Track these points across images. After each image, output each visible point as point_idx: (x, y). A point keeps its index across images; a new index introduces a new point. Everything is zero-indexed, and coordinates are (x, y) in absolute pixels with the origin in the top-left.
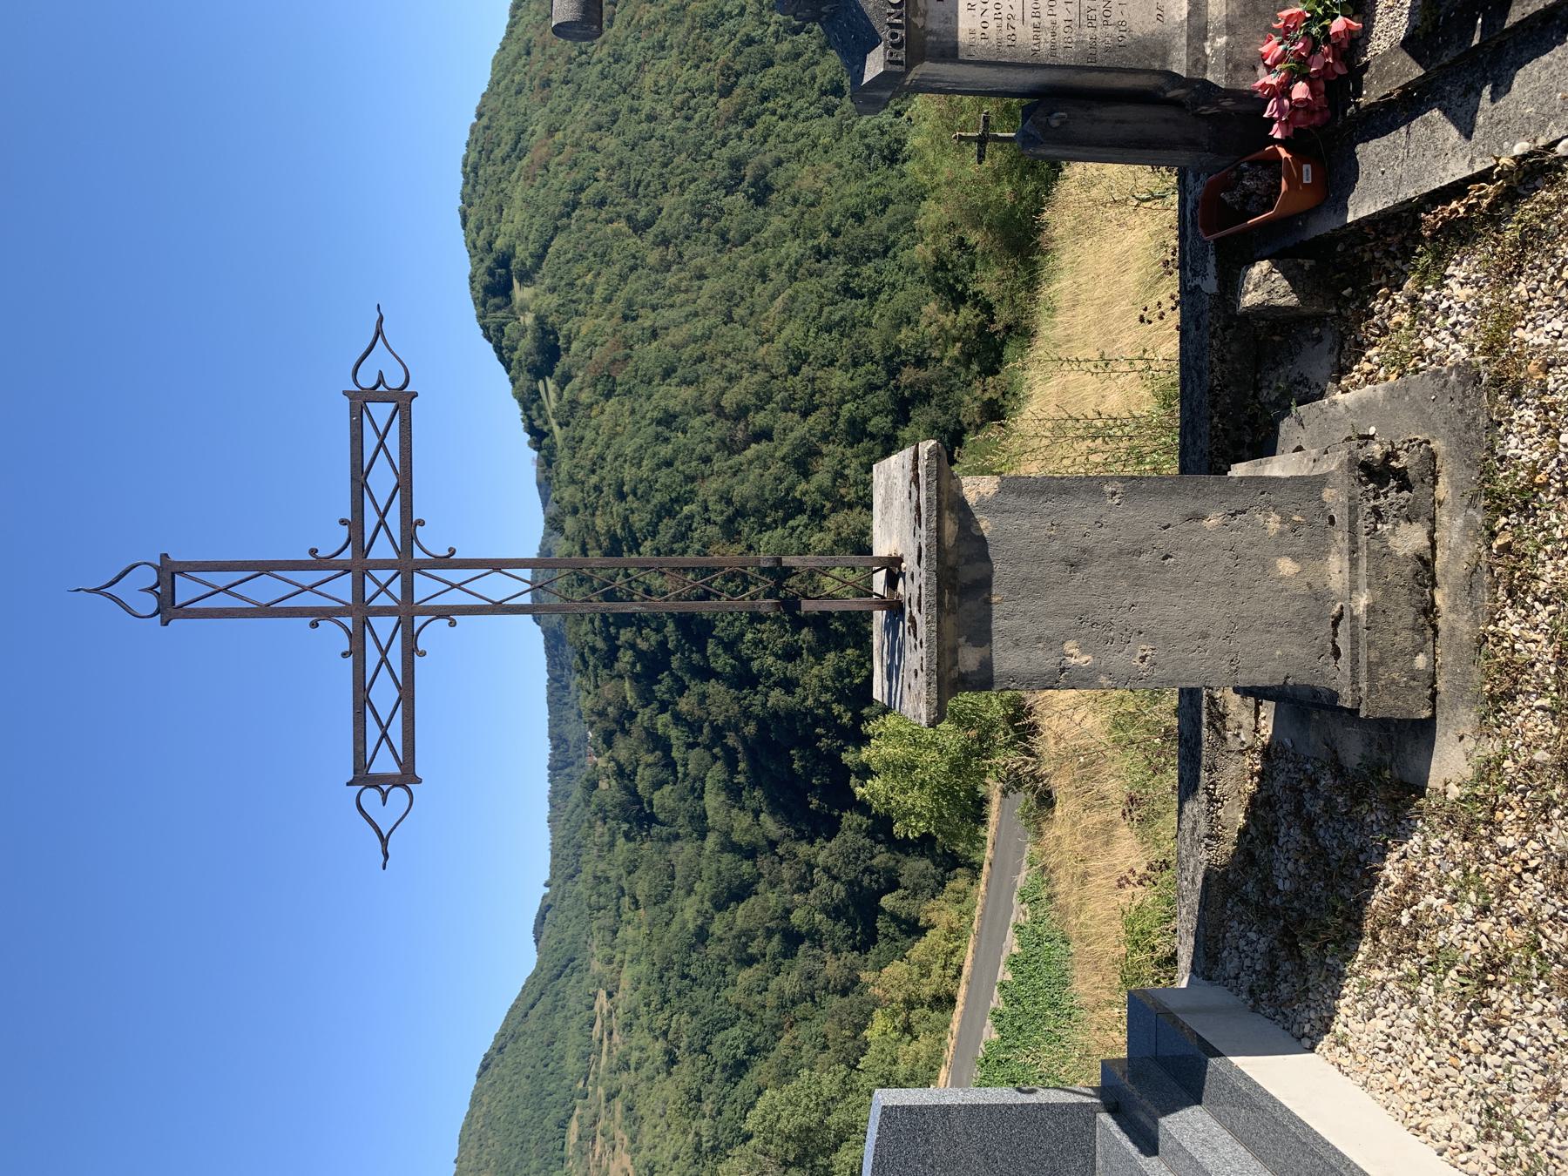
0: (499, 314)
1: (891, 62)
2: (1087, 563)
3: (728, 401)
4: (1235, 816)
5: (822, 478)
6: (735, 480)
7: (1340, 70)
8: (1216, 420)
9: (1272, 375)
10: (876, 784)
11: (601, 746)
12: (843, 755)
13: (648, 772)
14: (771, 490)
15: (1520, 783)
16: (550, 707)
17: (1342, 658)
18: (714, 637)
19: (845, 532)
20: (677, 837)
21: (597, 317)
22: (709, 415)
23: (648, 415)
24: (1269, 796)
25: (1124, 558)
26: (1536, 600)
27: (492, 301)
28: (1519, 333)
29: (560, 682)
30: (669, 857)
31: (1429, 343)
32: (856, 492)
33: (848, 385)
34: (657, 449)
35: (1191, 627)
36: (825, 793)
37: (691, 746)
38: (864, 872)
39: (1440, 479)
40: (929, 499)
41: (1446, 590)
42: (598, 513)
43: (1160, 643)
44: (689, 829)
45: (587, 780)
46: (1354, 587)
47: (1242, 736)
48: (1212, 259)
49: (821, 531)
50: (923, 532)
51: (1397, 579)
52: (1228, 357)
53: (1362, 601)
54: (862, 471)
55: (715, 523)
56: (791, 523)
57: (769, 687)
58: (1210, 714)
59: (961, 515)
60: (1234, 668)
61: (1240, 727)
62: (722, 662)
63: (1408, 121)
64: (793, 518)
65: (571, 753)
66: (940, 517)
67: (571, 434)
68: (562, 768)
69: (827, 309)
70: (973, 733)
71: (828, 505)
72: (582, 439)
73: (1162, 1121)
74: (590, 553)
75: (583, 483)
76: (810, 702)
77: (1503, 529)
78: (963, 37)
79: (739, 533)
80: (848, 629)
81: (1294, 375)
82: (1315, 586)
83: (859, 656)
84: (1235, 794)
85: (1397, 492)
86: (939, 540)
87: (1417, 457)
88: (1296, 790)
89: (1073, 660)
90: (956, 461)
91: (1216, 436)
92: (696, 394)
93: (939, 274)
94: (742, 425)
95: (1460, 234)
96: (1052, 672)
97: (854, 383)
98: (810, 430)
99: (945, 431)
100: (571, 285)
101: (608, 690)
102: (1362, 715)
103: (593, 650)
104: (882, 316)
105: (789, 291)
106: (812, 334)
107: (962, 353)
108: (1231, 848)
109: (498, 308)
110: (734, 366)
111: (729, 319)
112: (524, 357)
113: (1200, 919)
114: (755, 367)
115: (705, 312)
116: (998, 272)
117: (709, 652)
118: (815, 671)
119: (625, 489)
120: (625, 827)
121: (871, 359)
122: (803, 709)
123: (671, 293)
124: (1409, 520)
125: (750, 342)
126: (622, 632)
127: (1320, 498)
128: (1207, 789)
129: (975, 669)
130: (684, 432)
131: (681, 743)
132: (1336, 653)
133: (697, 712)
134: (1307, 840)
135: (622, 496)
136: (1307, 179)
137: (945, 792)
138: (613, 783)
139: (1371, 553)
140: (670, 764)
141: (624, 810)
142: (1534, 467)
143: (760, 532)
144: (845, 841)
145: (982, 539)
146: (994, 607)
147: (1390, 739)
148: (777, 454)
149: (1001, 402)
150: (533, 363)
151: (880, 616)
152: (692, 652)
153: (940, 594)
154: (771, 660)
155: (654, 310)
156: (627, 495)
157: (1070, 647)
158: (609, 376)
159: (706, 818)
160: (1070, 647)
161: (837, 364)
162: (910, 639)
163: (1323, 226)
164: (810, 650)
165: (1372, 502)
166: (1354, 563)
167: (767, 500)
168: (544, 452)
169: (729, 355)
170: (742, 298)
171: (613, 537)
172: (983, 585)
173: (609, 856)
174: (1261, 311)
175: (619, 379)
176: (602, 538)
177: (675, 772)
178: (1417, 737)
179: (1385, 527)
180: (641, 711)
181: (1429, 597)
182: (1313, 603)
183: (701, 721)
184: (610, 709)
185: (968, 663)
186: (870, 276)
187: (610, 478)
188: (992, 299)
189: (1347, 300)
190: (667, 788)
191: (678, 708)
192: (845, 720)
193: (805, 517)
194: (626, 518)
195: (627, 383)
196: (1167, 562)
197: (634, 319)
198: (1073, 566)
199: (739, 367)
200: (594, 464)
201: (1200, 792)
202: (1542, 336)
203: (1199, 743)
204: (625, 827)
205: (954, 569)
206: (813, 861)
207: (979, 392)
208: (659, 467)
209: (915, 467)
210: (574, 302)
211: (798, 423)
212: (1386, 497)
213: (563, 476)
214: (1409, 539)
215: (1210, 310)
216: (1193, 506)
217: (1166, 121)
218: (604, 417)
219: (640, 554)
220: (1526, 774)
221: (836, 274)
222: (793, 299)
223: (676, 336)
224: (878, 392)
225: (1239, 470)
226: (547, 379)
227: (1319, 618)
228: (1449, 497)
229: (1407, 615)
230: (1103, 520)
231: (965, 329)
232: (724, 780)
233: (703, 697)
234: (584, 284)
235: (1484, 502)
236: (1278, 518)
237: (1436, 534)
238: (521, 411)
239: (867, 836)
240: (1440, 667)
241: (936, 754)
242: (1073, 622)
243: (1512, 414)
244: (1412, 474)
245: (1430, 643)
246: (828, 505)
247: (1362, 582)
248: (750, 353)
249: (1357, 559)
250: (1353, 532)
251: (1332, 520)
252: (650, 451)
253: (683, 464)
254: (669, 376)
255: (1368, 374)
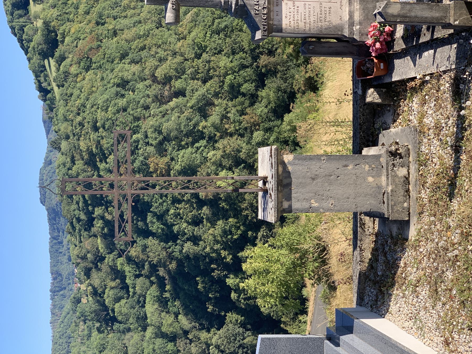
0: (21, 20)
1: (263, 35)
2: (317, 178)
3: (159, 73)
4: (368, 255)
5: (214, 118)
6: (164, 120)
7: (389, 39)
8: (361, 133)
9: (378, 120)
10: (250, 282)
11: (83, 277)
12: (227, 280)
13: (111, 292)
14: (185, 125)
16: (51, 255)
18: (151, 212)
19: (228, 150)
20: (129, 330)
21: (81, 23)
22: (148, 81)
23: (112, 81)
27: (17, 12)
29: (57, 240)
30: (124, 342)
32: (235, 127)
33: (229, 65)
34: (117, 101)
35: (345, 196)
36: (217, 302)
37: (137, 276)
38: (239, 348)
40: (275, 162)
42: (81, 139)
43: (336, 200)
44: (136, 325)
45: (74, 298)
46: (388, 185)
48: (360, 84)
49: (214, 150)
50: (273, 170)
51: (399, 183)
52: (365, 114)
53: (390, 188)
54: (238, 114)
55: (152, 145)
56: (197, 145)
57: (184, 241)
58: (360, 223)
62: (156, 227)
63: (404, 57)
64: (197, 141)
65: (63, 282)
66: (278, 166)
67: (65, 91)
68: (58, 291)
69: (217, 21)
70: (298, 255)
71: (218, 134)
72: (71, 95)
73: (342, 337)
74: (76, 162)
75: (72, 121)
76: (208, 249)
78: (284, 26)
79: (166, 151)
80: (230, 206)
81: (383, 121)
83: (236, 223)
86: (278, 172)
87: (404, 150)
88: (383, 245)
89: (313, 205)
90: (291, 111)
92: (140, 69)
94: (167, 87)
95: (415, 90)
96: (308, 208)
99: (285, 92)
101: (88, 244)
103: (79, 220)
107: (294, 51)
108: (367, 265)
109: (21, 16)
111: (159, 25)
112: (36, 46)
113: (358, 288)
114: (175, 54)
117: (148, 221)
118: (211, 231)
119: (98, 124)
120: (98, 325)
121: (243, 50)
122: (204, 254)
123: (125, 9)
125: (172, 39)
126: (96, 209)
130: (133, 91)
131: (131, 274)
132: (384, 203)
133: (141, 256)
135: (96, 129)
136: (382, 67)
137: (284, 284)
138: (91, 299)
139: (392, 175)
140: (125, 287)
143: (178, 150)
144: (228, 330)
148: (188, 105)
149: (316, 78)
151: (261, 194)
152: (138, 221)
153: (278, 187)
154: (185, 225)
155: (115, 19)
156: (99, 128)
158: (88, 58)
159: (146, 318)
160: (313, 201)
161: (223, 53)
162: (270, 200)
163: (387, 80)
164: (208, 219)
165: (392, 162)
166: (388, 178)
167: (182, 131)
168: (48, 102)
169: (159, 46)
171: (91, 154)
172: (290, 184)
173: (88, 343)
174: (371, 104)
176: (84, 154)
177: (128, 292)
180: (107, 256)
183: (143, 261)
184: (89, 255)
187: (89, 118)
189: (396, 101)
190: (123, 301)
191: (130, 254)
192: (228, 260)
193: (205, 141)
194: (99, 142)
195: (99, 62)
197: (103, 24)
199: (166, 53)
200: (79, 109)
203: (357, 233)
204: (98, 325)
205: (282, 180)
206: (209, 342)
207: (303, 73)
208: (118, 111)
209: (271, 153)
210: (67, 14)
213: (60, 116)
214: (402, 172)
216: (345, 163)
217: (344, 47)
218: (85, 82)
219: (107, 163)
223: (128, 34)
224: (247, 70)
226: (50, 59)
227: (379, 193)
229: (402, 192)
232: (157, 296)
233: (145, 247)
234: (73, 3)
235: (417, 163)
238: (34, 77)
239: (241, 326)
241: (280, 266)
244: (403, 155)
246: (218, 134)
247: (390, 183)
248: (172, 45)
251: (382, 167)
252: (113, 102)
253: (133, 110)
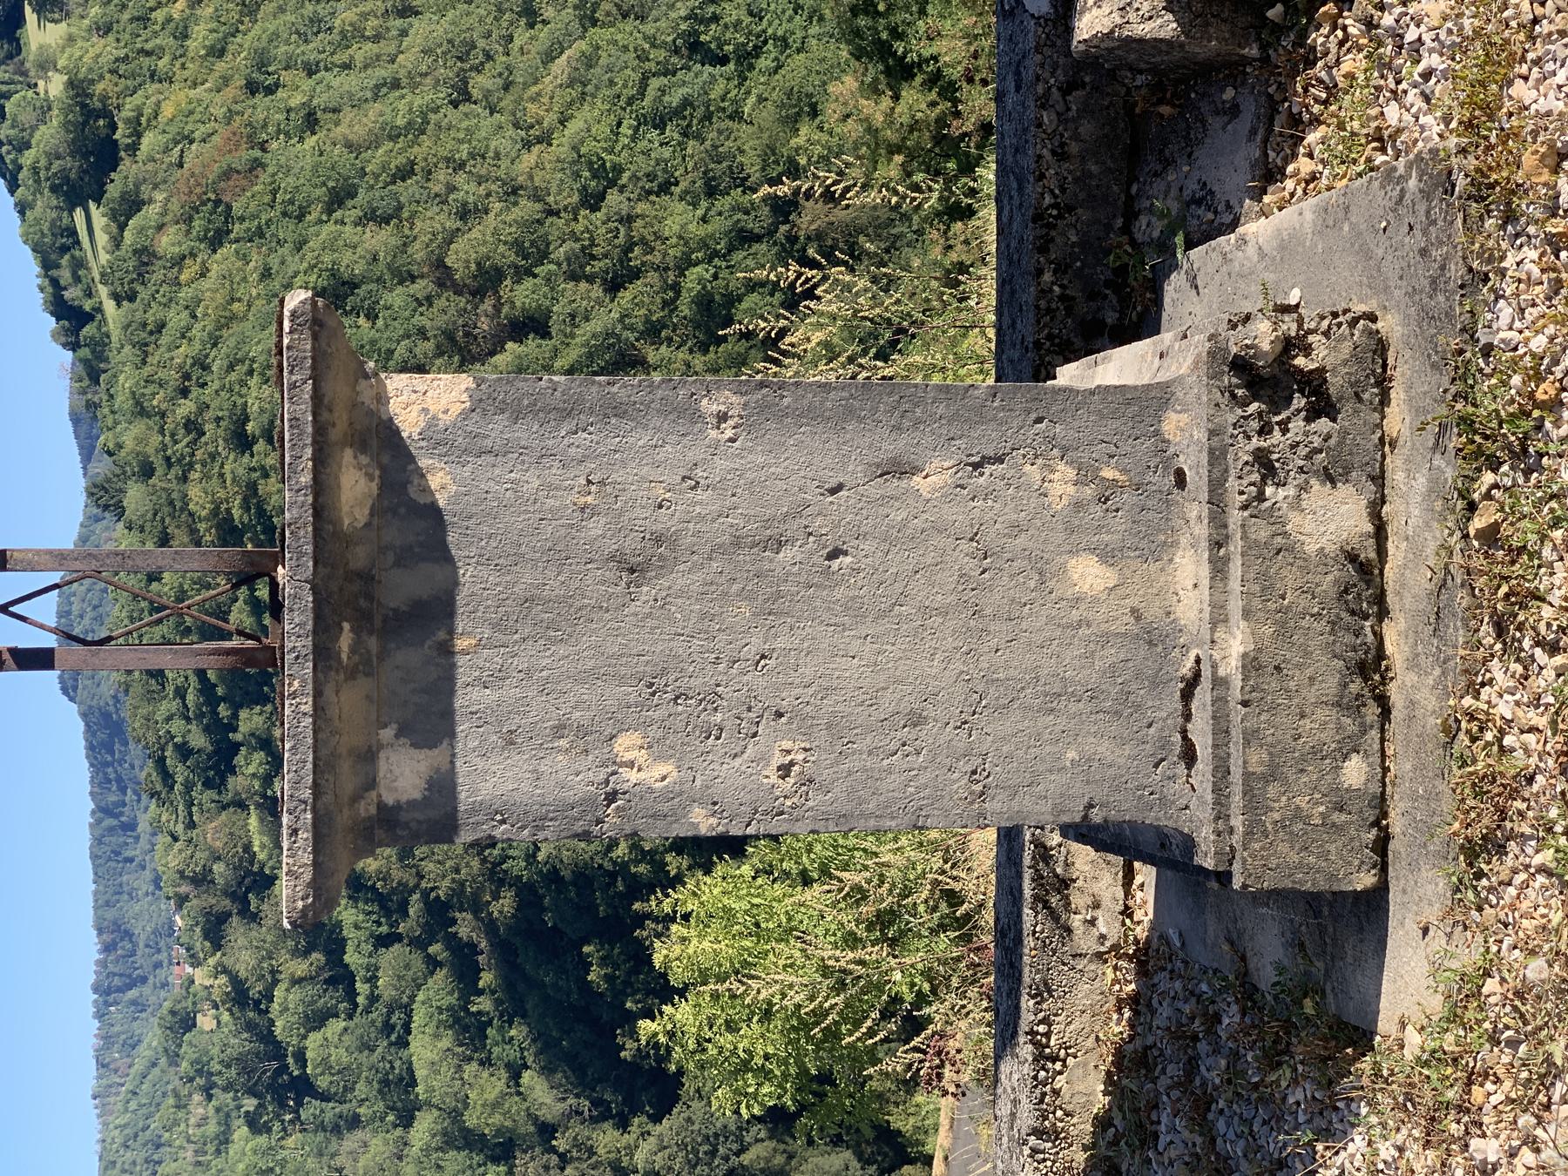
2: (665, 566)
3: (461, 257)
8: (1047, 277)
9: (1158, 186)
11: (200, 944)
13: (295, 996)
15: (1507, 1027)
16: (96, 867)
17: (1199, 766)
20: (354, 1122)
21: (195, 85)
22: (421, 283)
24: (1147, 1048)
25: (744, 556)
26: (1537, 644)
28: (1520, 90)
29: (117, 816)
30: (338, 1161)
31: (1393, 113)
33: (696, 230)
35: (888, 703)
37: (383, 942)
39: (1393, 394)
41: (1402, 625)
42: (194, 475)
43: (821, 737)
44: (380, 1106)
45: (173, 1013)
46: (1218, 618)
47: (1100, 922)
51: (1304, 602)
52: (1074, 148)
53: (1235, 645)
58: (1038, 878)
59: (385, 459)
60: (978, 788)
61: (1096, 905)
67: (139, 315)
68: (120, 990)
69: (655, 83)
72: (161, 326)
75: (163, 415)
77: (1488, 496)
81: (1192, 186)
82: (1148, 616)
84: (1090, 1042)
85: (1308, 420)
87: (1346, 349)
89: (633, 776)
91: (1049, 310)
92: (394, 241)
93: (862, 22)
94: (487, 305)
96: (588, 801)
97: (710, 228)
98: (623, 317)
100: (143, 20)
101: (213, 831)
102: (1237, 883)
103: (184, 751)
104: (761, 99)
105: (582, 45)
106: (624, 130)
110: (472, 187)
111: (461, 95)
112: (43, 163)
114: (512, 192)
115: (414, 81)
116: (967, 20)
119: (250, 427)
122: (608, 865)
123: (345, 41)
124: (1329, 478)
125: (504, 142)
126: (243, 714)
127: (1157, 433)
128: (1032, 1033)
129: (417, 795)
130: (372, 316)
131: (362, 935)
133: (397, 874)
134: (1199, 1140)
135: (243, 442)
138: (226, 1017)
139: (1250, 546)
140: (341, 978)
141: (247, 1070)
142: (1536, 368)
144: (689, 1120)
145: (434, 512)
146: (461, 660)
147: (1322, 930)
148: (558, 364)
150: (64, 174)
155: (310, 74)
156: (254, 441)
157: (627, 745)
158: (218, 202)
159: (413, 1082)
161: (677, 190)
166: (1219, 568)
168: (85, 352)
169: (462, 165)
170: (489, 57)
173: (218, 1163)
175: (237, 208)
176: (202, 526)
177: (351, 994)
178: (1361, 930)
179: (1282, 492)
181: (1370, 638)
182: (1143, 650)
183: (405, 891)
184: (218, 868)
185: (400, 784)
186: (739, 22)
187: (219, 405)
188: (955, 73)
190: (335, 1026)
194: (252, 487)
195: (254, 217)
196: (835, 564)
197: (270, 90)
198: (635, 570)
199: (482, 190)
200: (187, 377)
201: (1022, 1039)
202: (1551, 94)
204: (250, 1104)
210: (148, 54)
211: (600, 303)
212: (1285, 431)
213: (122, 400)
215: (1038, 49)
216: (891, 446)
218: (206, 284)
220: (1515, 1008)
221: (673, 15)
222: (589, 61)
223: (354, 125)
224: (756, 247)
225: (1068, 375)
226: (92, 205)
227: (1156, 684)
228: (1406, 432)
230: (699, 472)
231: (912, 129)
232: (450, 1008)
234: (169, 20)
236: (1071, 473)
237: (1386, 509)
238: (37, 269)
240: (1393, 784)
242: (631, 693)
243: (1503, 258)
245: (1374, 734)
247: (1235, 606)
248: (504, 163)
249: (1227, 560)
250: (1217, 502)
251: (1180, 479)
254: (341, 204)
255: (1307, 183)
